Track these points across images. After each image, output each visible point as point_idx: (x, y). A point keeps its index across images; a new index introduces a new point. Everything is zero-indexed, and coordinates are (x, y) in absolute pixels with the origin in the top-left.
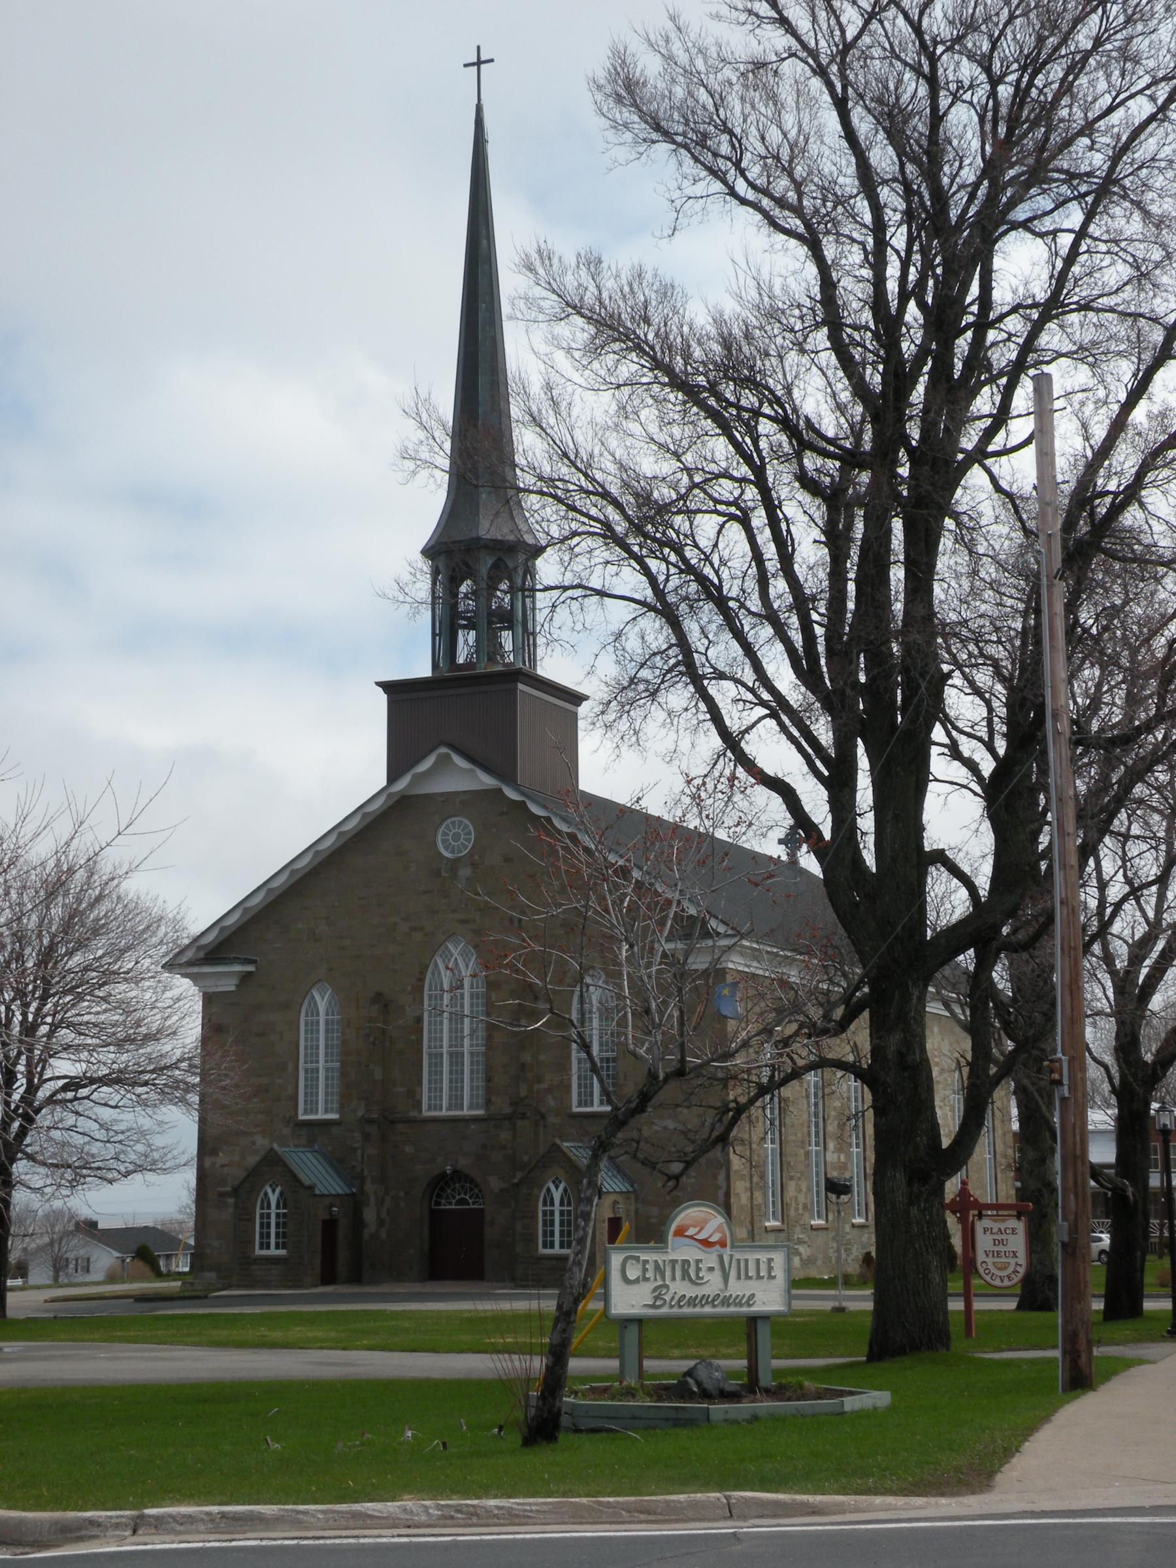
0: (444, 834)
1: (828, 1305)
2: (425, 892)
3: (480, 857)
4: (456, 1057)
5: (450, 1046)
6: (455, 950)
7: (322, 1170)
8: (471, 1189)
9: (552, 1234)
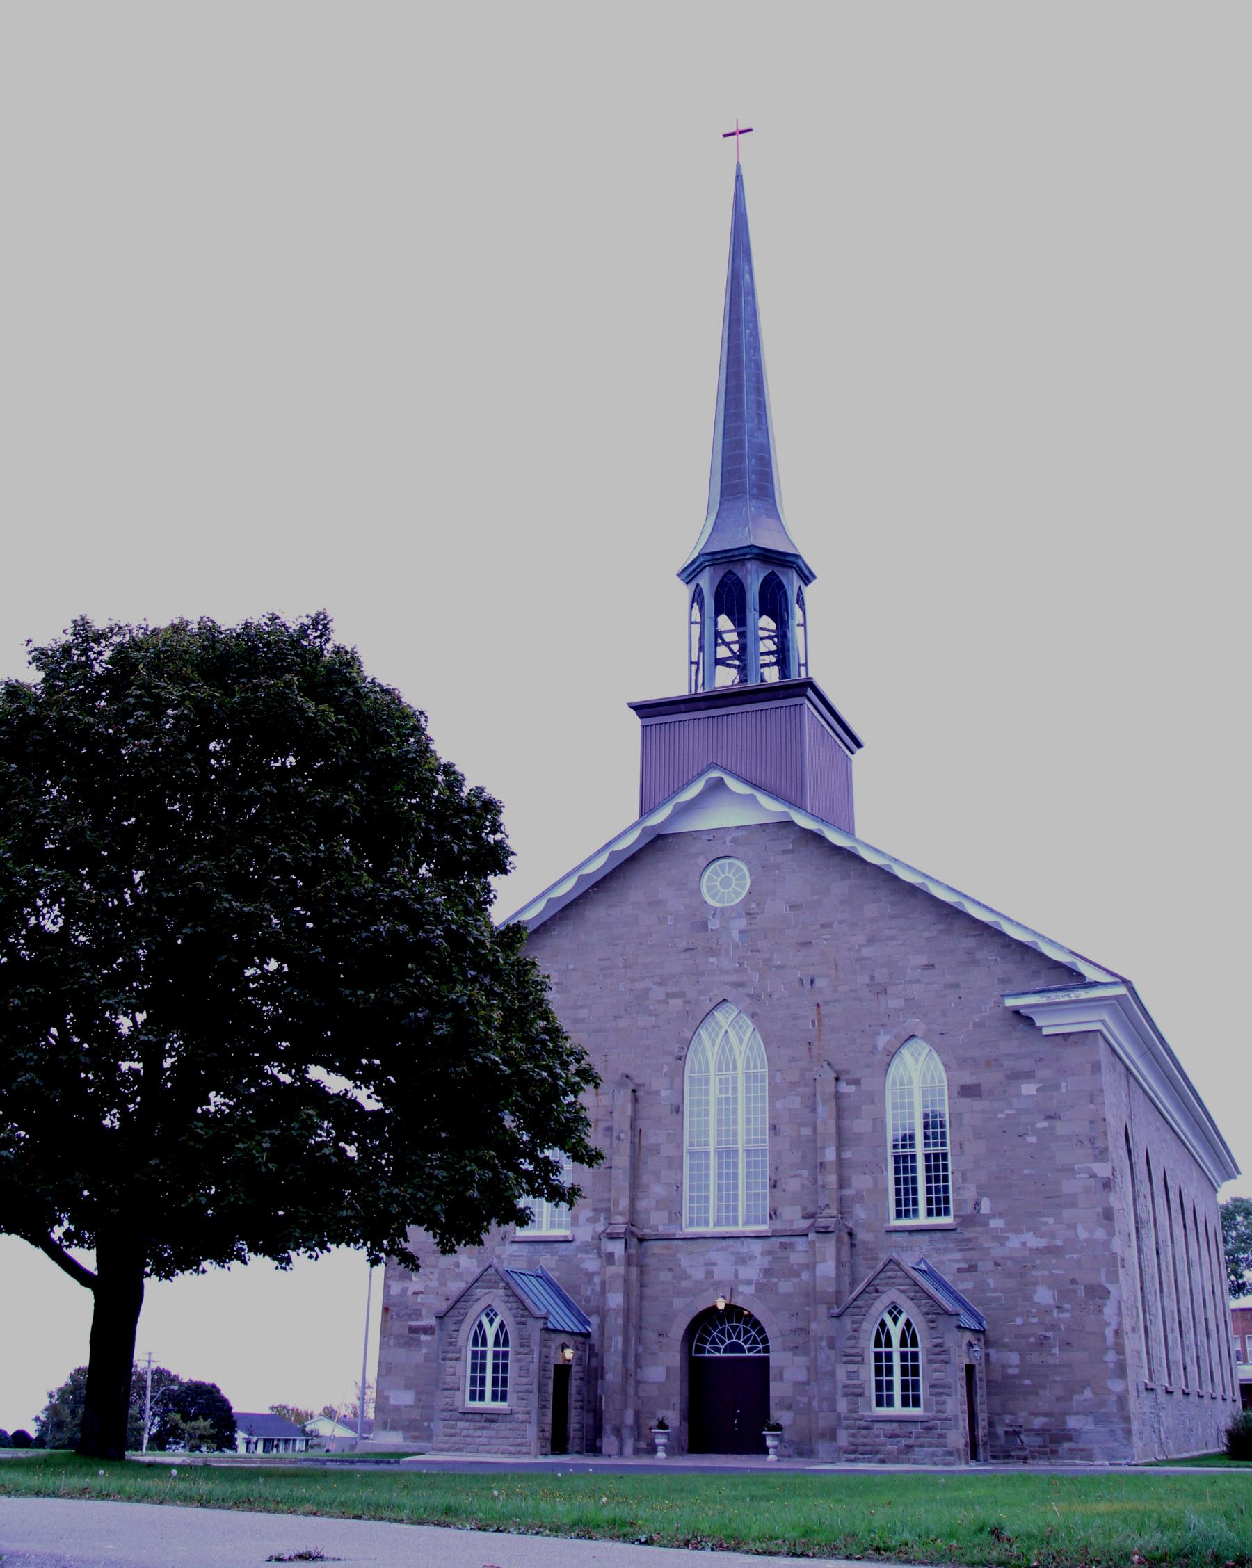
0: (710, 880)
1: (967, 1517)
2: (686, 950)
3: (758, 905)
4: (727, 1155)
5: (719, 1142)
6: (723, 1018)
7: (551, 1301)
8: (746, 1332)
9: (890, 1385)
